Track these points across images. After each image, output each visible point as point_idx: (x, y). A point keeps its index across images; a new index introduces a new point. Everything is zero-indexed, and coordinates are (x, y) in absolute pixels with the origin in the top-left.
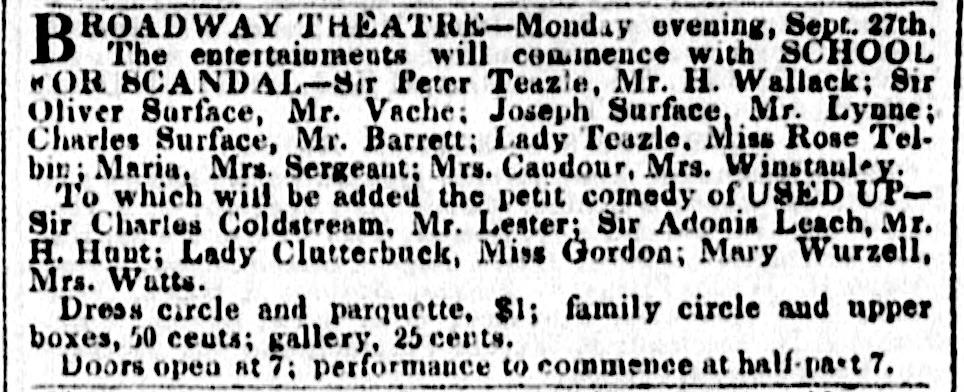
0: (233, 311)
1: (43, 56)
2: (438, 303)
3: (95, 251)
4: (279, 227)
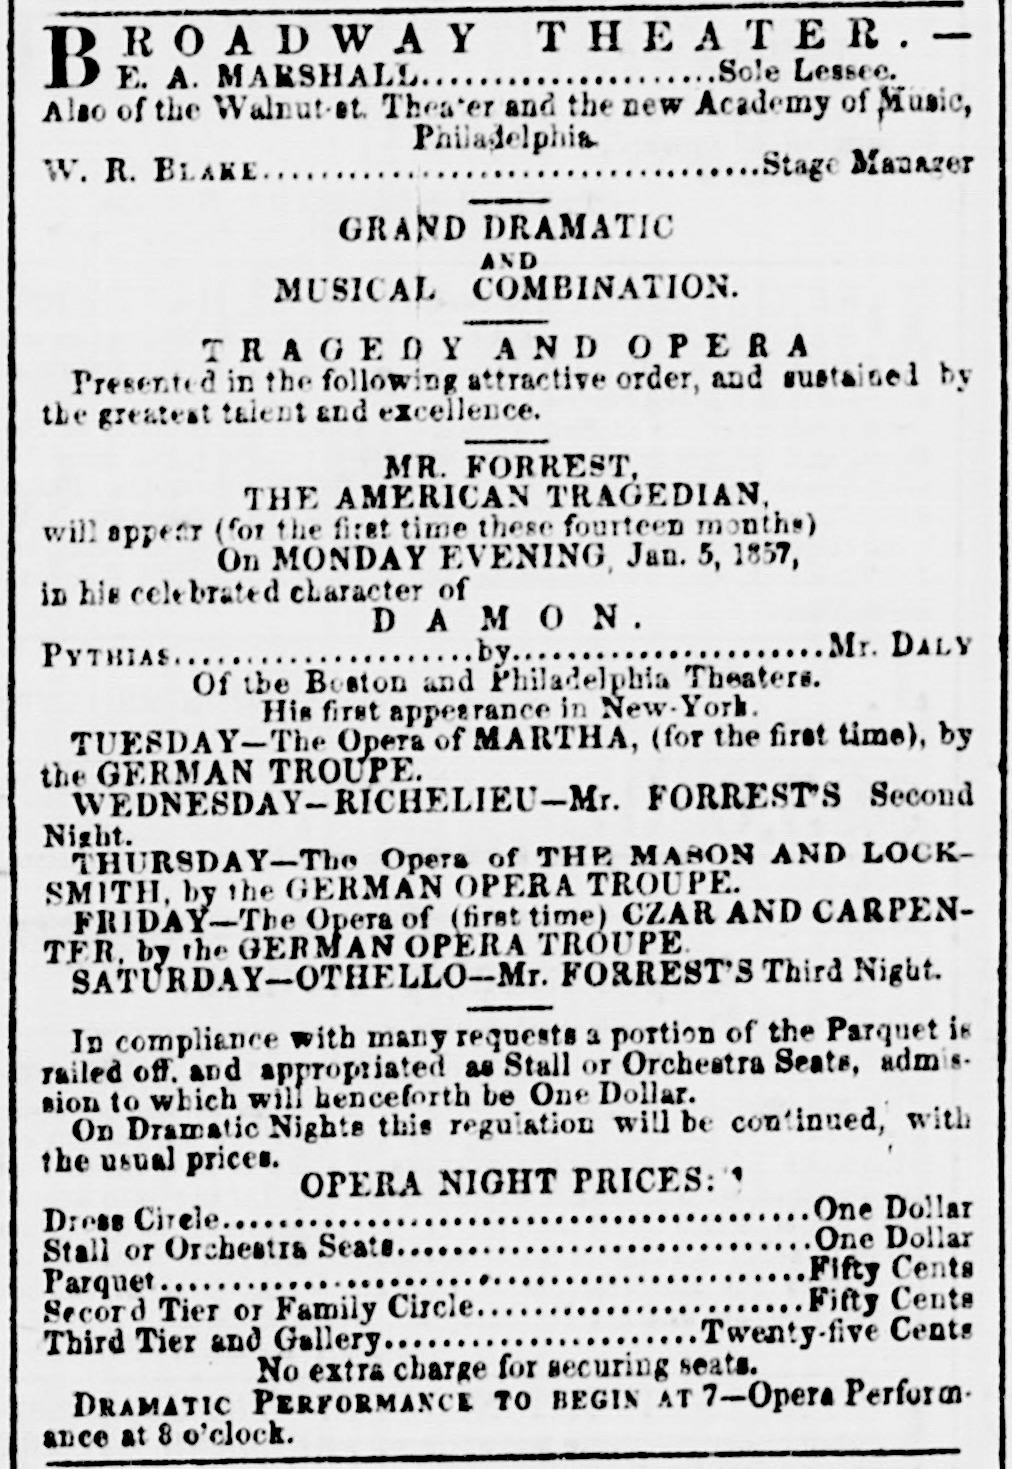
0: (558, 1398)
1: (60, 79)
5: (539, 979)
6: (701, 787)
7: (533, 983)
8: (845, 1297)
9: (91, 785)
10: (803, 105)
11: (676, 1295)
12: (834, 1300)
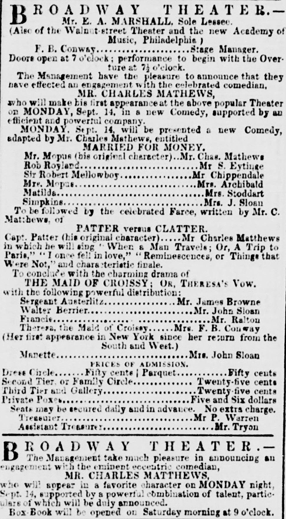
5: (189, 303)
7: (187, 304)
8: (239, 372)
9: (114, 241)
10: (266, 32)
11: (168, 317)
12: (236, 372)
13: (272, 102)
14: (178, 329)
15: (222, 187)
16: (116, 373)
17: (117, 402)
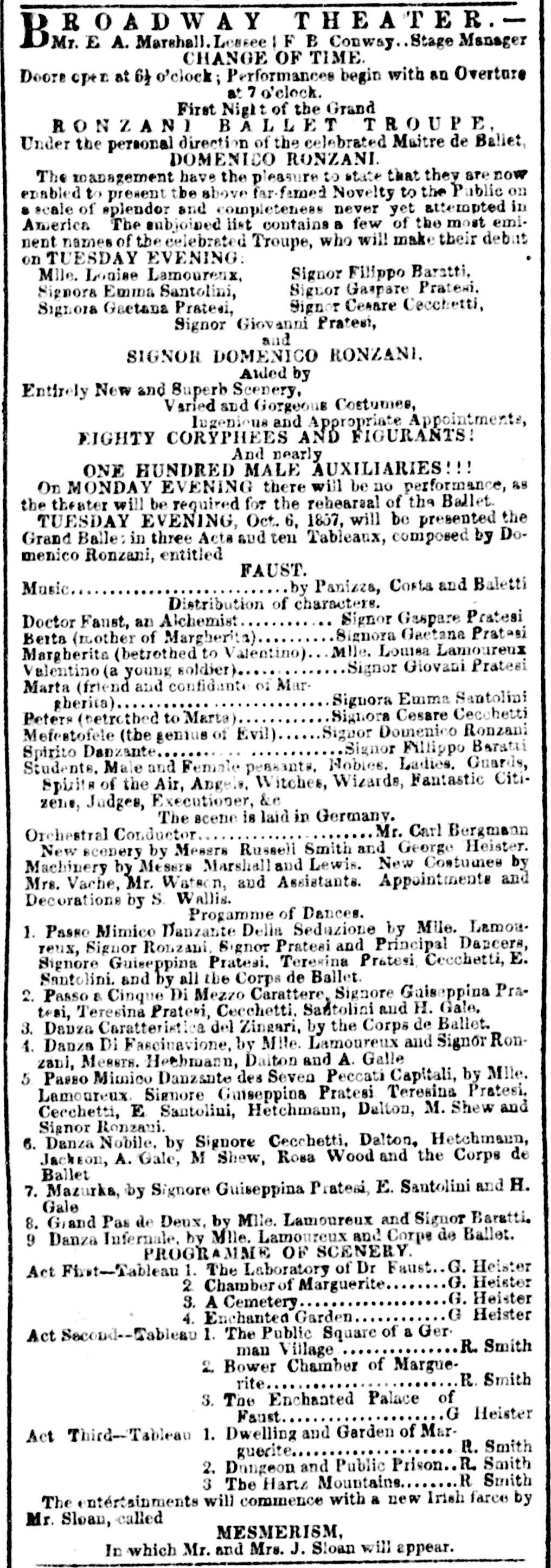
2: (330, 1136)
3: (476, 845)
4: (455, 143)
6: (197, 465)
13: (340, 1185)
14: (252, 473)
15: (280, 886)
16: (345, 914)
17: (268, 721)
